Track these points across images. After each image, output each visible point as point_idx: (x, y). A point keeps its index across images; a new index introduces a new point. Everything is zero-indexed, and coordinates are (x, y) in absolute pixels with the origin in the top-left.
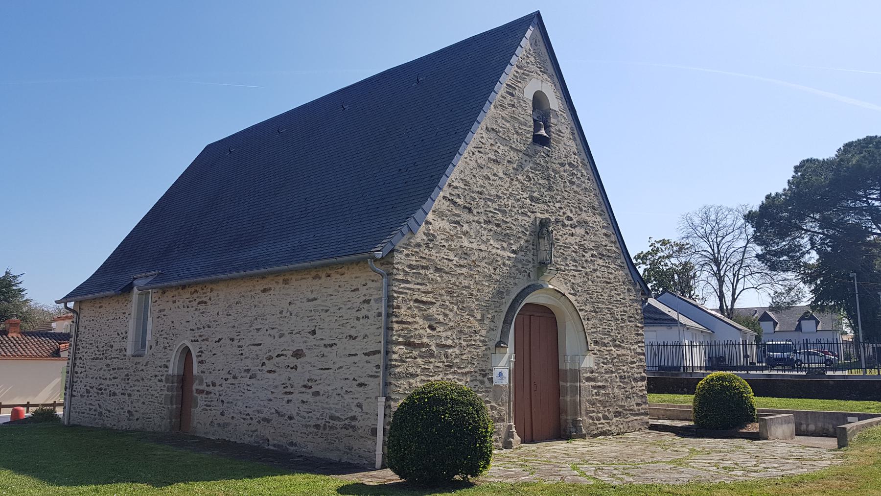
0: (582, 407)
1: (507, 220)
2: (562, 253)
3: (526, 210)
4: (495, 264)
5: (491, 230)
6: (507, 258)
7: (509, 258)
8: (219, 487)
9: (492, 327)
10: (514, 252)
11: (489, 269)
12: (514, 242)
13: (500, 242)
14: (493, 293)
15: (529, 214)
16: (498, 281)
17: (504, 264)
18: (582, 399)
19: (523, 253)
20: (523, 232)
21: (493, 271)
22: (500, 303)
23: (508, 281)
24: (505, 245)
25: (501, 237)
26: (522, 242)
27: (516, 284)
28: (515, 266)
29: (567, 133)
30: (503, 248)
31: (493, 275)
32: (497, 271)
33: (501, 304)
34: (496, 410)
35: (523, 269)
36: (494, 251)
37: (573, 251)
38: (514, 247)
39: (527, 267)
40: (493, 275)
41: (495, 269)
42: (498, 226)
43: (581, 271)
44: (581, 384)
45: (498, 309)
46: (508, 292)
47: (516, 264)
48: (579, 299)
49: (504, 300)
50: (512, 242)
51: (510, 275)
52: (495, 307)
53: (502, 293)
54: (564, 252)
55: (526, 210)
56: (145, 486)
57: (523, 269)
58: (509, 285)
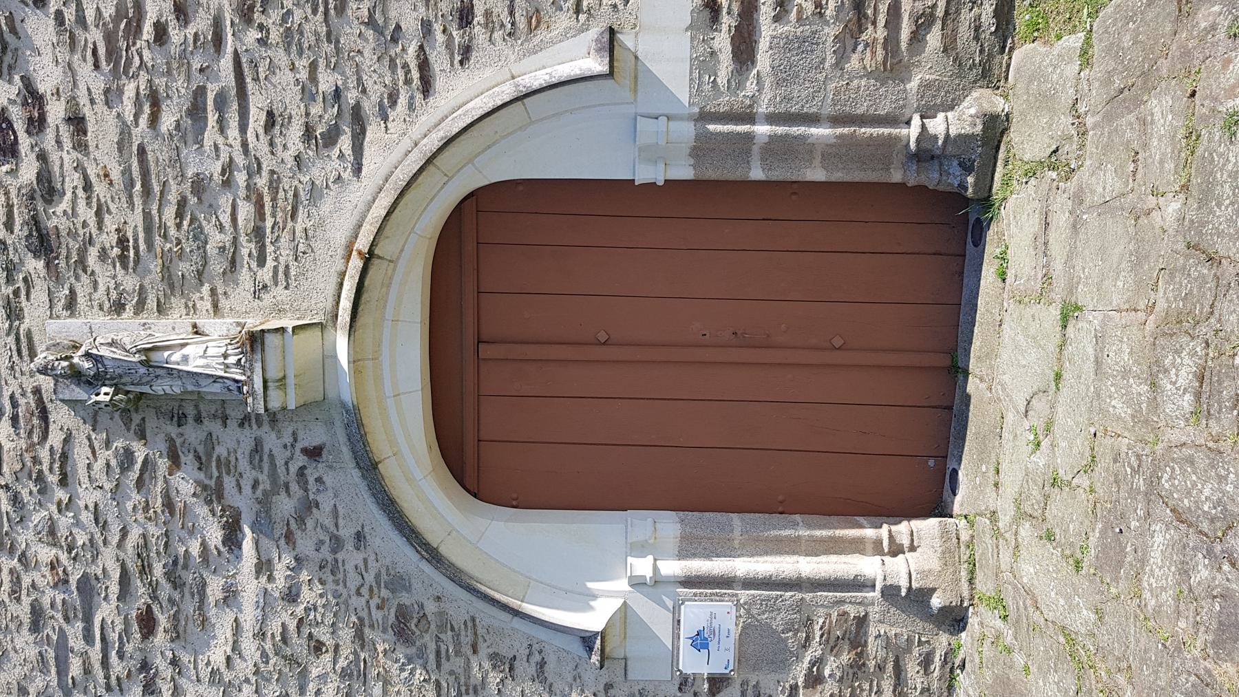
0: (860, 110)
1: (116, 575)
2: (180, 215)
3: (44, 454)
4: (299, 646)
5: (174, 662)
6: (264, 579)
7: (263, 567)
8: (419, 299)
9: (532, 670)
10: (232, 539)
11: (323, 677)
12: (192, 532)
13: (212, 612)
14: (410, 660)
15: (55, 439)
16: (359, 636)
17: (291, 596)
18: (828, 110)
19: (229, 482)
20: (140, 484)
21: (327, 658)
22: (441, 628)
23: (353, 581)
24: (215, 588)
25: (189, 607)
26: (185, 485)
27: (359, 537)
28: (289, 537)
29: (253, 111)
30: (230, 596)
31: (342, 663)
32: (323, 634)
33: (445, 624)
34: (819, 662)
35: (294, 487)
36: (249, 646)
37: (154, 120)
38: (215, 536)
39: (280, 462)
40: (342, 663)
41: (318, 648)
42: (147, 623)
43: (236, 53)
44: (763, 108)
45: (466, 639)
46: (398, 583)
47: (280, 530)
48: (376, 92)
49: (431, 607)
50: (195, 548)
51: (330, 569)
52: (458, 653)
53: (403, 615)
54: (173, 197)
55: (44, 454)
56: (364, 160)
57: (294, 487)
58: (370, 578)
